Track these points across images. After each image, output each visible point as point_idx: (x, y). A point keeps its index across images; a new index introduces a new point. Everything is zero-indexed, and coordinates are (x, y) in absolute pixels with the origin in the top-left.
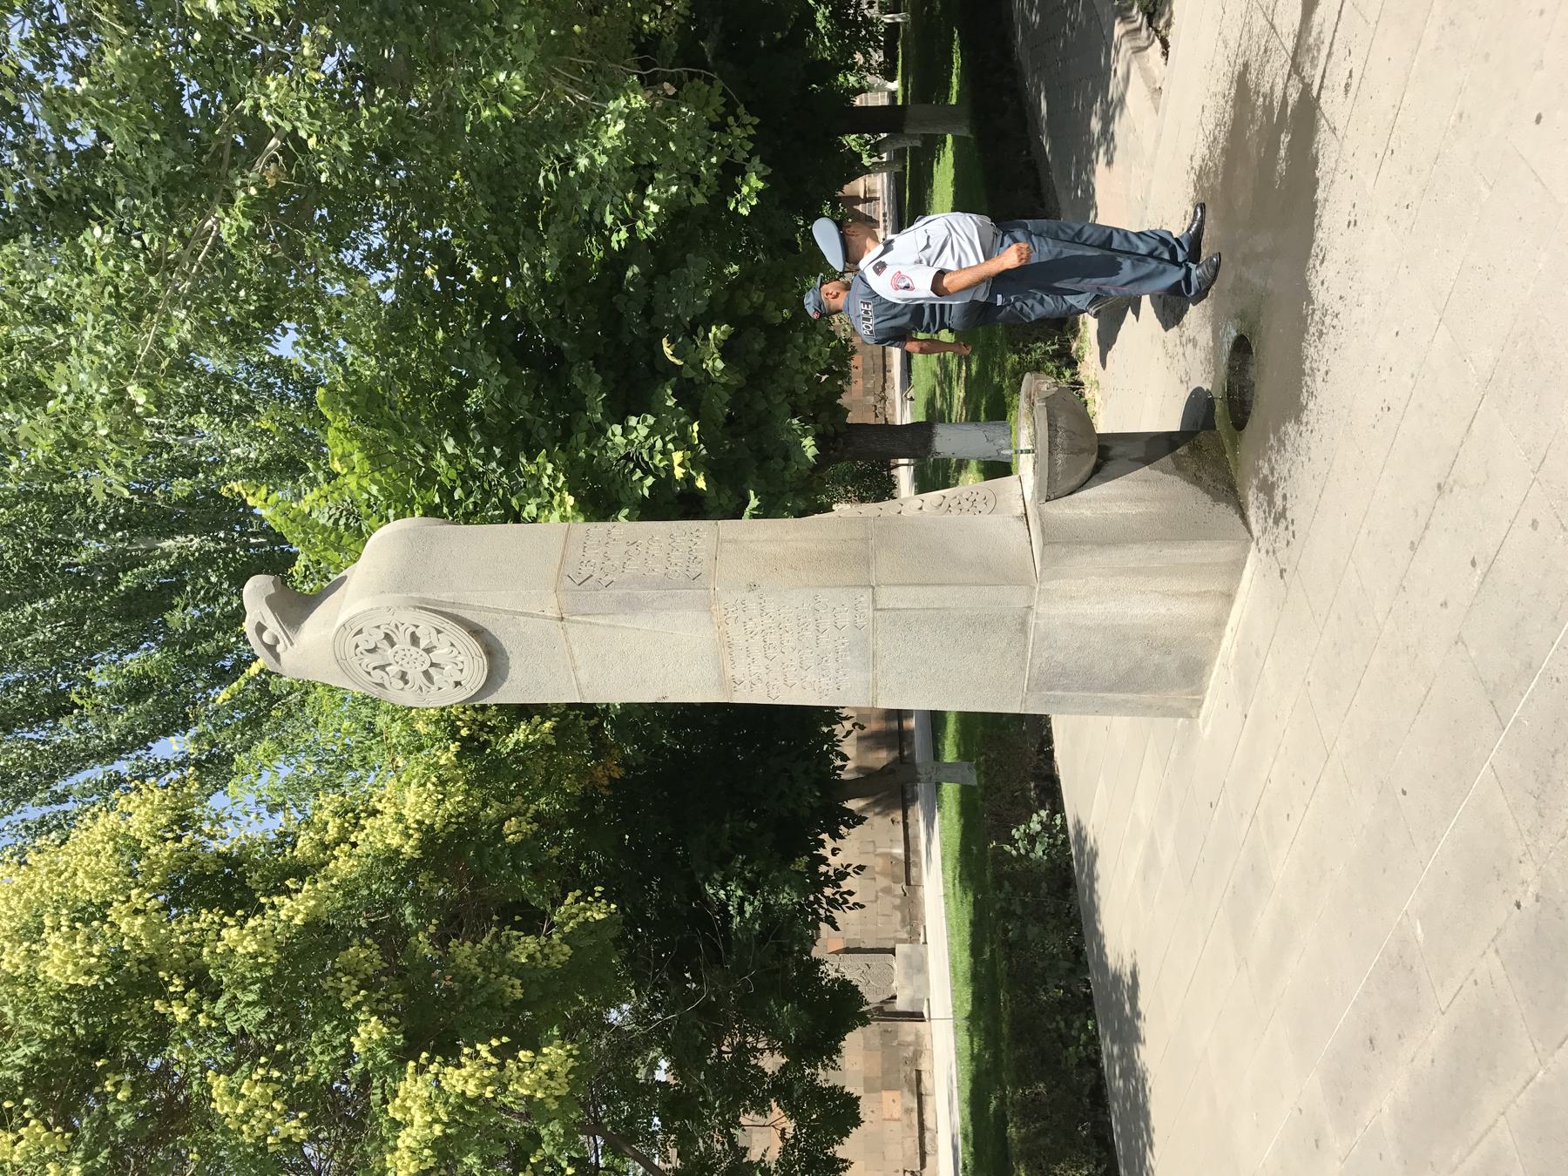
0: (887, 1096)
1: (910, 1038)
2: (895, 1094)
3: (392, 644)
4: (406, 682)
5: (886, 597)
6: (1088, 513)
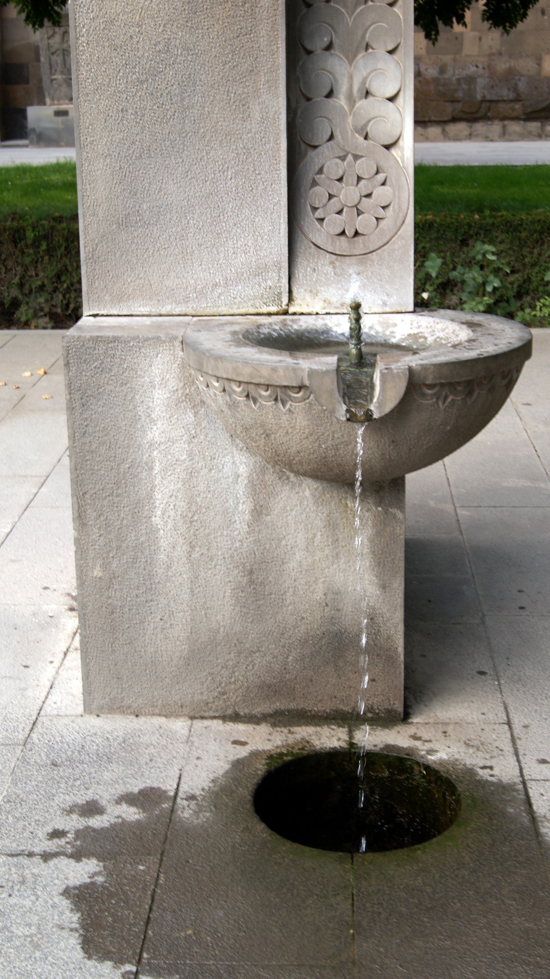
6: (155, 433)
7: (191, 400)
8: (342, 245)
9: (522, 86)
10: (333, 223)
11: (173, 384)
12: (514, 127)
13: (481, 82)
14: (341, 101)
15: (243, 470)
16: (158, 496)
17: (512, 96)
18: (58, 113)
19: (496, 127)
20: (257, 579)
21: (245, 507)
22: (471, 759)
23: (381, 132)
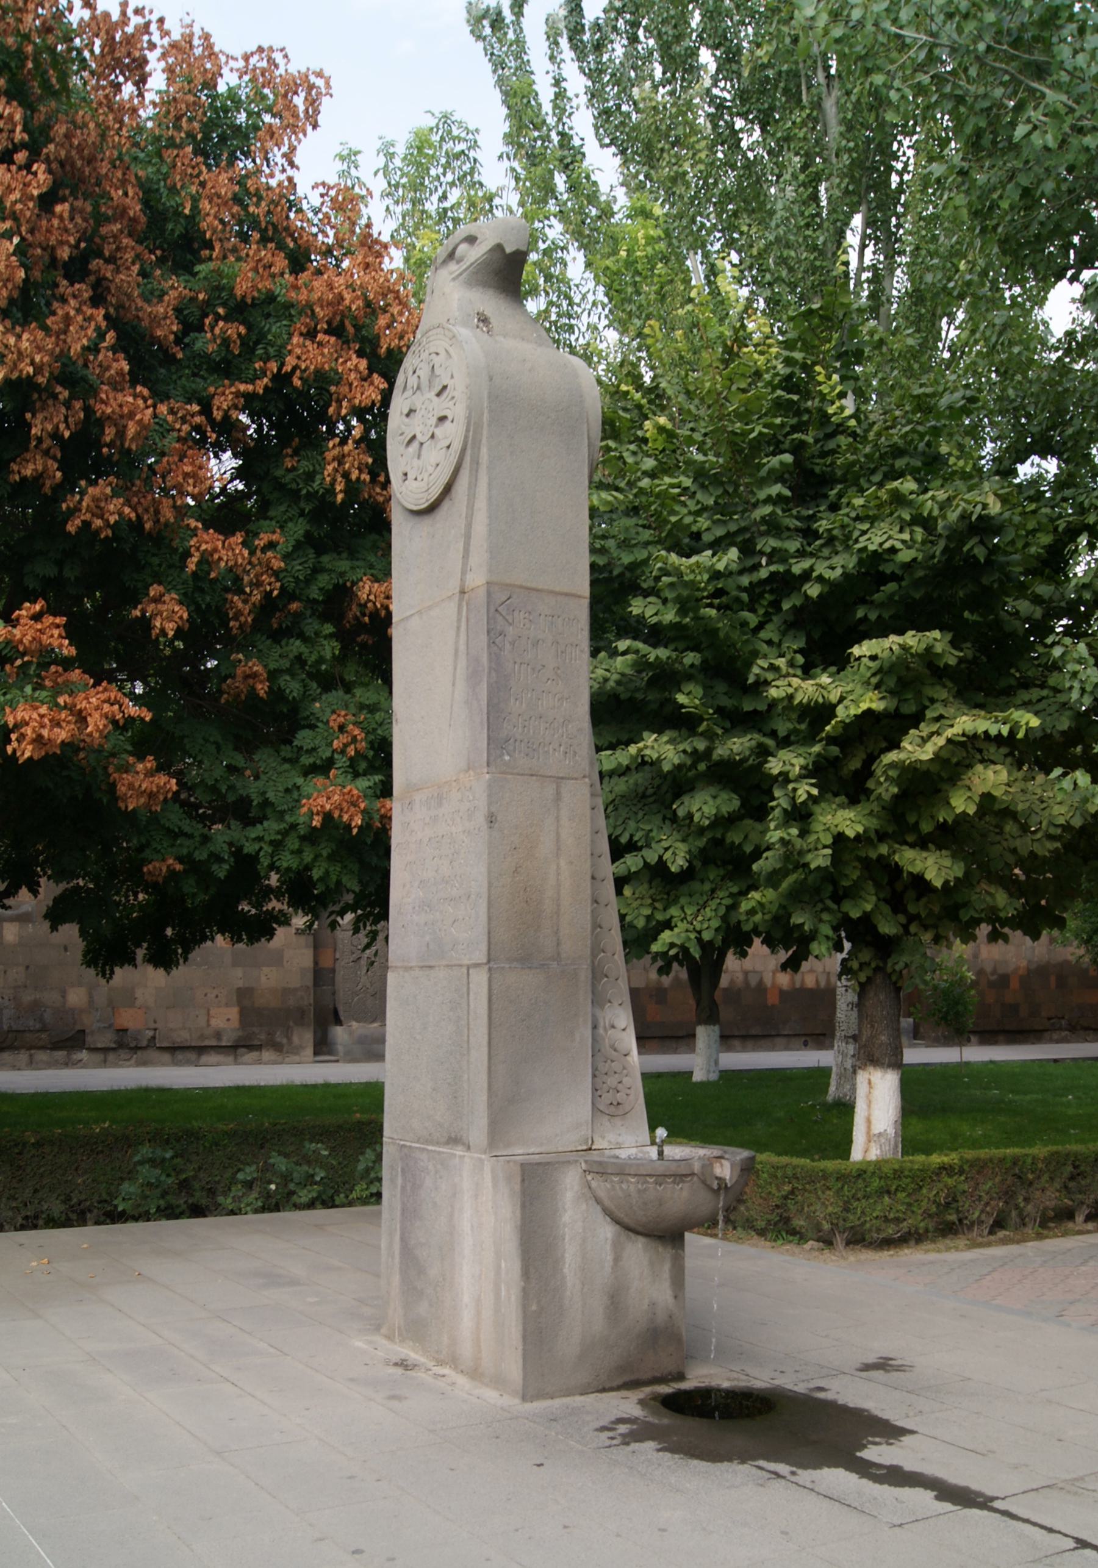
0: (233, 1013)
1: (296, 1039)
3: (438, 395)
4: (408, 415)
5: (480, 979)
8: (612, 1109)
9: (48, 1017)
11: (576, 1188)
12: (42, 1056)
15: (609, 1235)
17: (38, 1026)
19: (23, 1056)
20: (615, 1300)
21: (610, 1258)
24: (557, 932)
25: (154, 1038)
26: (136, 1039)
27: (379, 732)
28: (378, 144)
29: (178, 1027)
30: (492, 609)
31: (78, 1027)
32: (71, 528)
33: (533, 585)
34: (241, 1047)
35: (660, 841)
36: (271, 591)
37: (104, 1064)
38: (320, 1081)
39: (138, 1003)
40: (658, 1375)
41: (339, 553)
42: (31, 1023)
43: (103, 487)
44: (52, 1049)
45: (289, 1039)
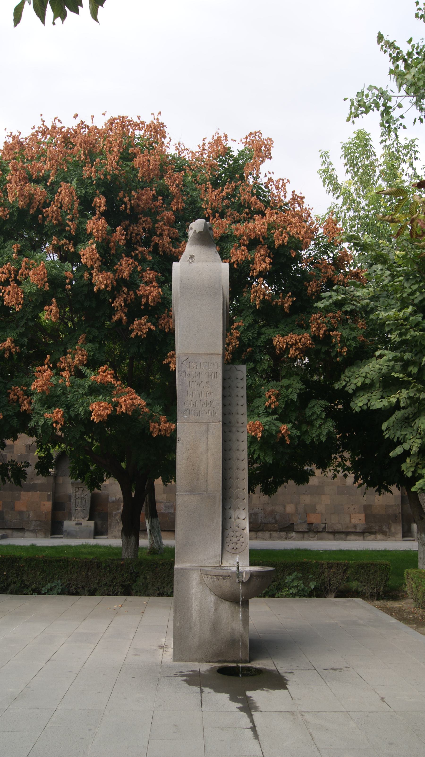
0: (362, 516)
1: (393, 529)
2: (363, 521)
6: (193, 591)
7: (202, 582)
8: (233, 551)
9: (278, 517)
10: (231, 546)
12: (275, 534)
13: (260, 515)
14: (233, 520)
15: (213, 599)
16: (193, 606)
17: (273, 521)
18: (77, 524)
19: (267, 534)
20: (215, 626)
21: (213, 609)
22: (265, 667)
23: (242, 526)
24: (207, 481)
25: (325, 527)
26: (317, 528)
27: (290, 397)
28: (341, 145)
29: (336, 522)
30: (180, 363)
31: (291, 522)
32: (132, 336)
33: (198, 352)
34: (365, 532)
35: (411, 439)
36: (236, 345)
37: (303, 538)
38: (383, 549)
39: (318, 511)
40: (236, 659)
41: (270, 326)
42: (271, 520)
43: (143, 320)
44: (279, 531)
45: (390, 529)
